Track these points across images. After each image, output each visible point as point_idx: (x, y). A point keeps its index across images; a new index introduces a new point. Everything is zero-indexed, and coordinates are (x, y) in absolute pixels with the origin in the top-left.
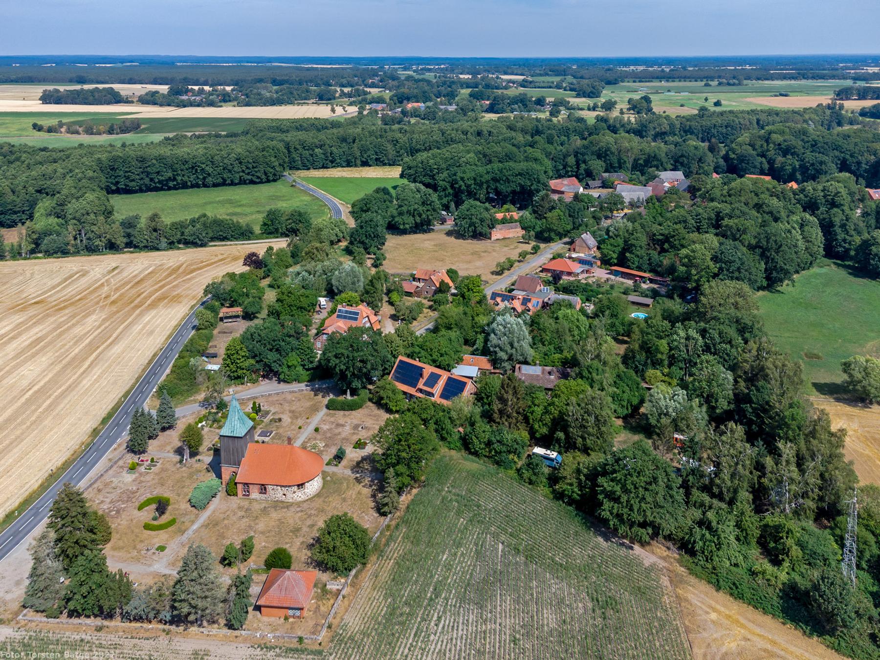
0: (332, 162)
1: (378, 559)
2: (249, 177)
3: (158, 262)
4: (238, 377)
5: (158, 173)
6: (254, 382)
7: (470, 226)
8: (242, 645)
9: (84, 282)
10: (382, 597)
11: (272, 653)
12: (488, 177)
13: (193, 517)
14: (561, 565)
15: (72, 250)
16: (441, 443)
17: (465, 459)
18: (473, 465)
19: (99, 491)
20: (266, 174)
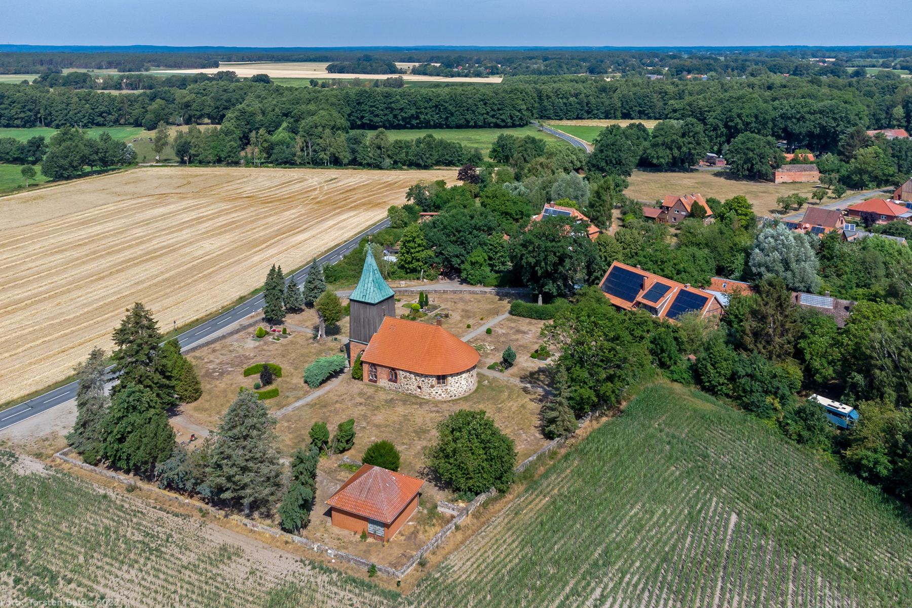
0: (588, 112)
1: (526, 491)
2: (494, 120)
3: (376, 177)
4: (414, 270)
5: (402, 109)
6: (432, 279)
7: (745, 163)
8: (289, 556)
9: (297, 187)
10: (517, 543)
11: (325, 578)
12: (776, 114)
13: (301, 393)
14: (848, 571)
15: (299, 161)
16: (659, 370)
17: (694, 395)
18: (706, 404)
19: (214, 351)
20: (511, 118)
